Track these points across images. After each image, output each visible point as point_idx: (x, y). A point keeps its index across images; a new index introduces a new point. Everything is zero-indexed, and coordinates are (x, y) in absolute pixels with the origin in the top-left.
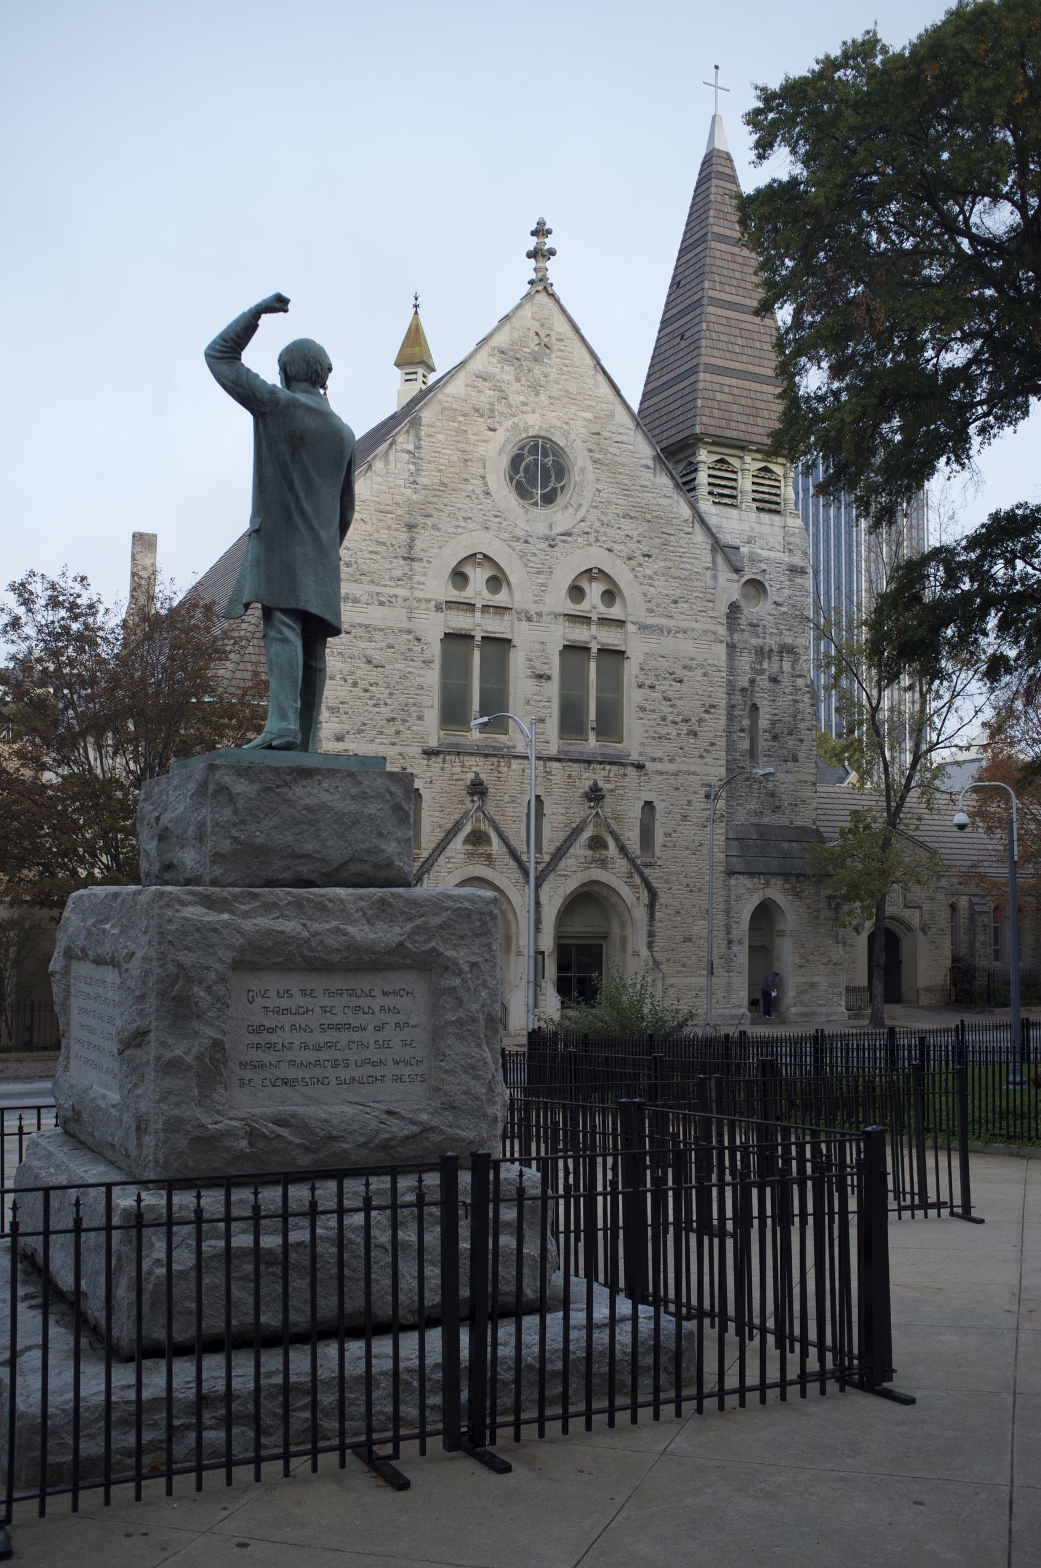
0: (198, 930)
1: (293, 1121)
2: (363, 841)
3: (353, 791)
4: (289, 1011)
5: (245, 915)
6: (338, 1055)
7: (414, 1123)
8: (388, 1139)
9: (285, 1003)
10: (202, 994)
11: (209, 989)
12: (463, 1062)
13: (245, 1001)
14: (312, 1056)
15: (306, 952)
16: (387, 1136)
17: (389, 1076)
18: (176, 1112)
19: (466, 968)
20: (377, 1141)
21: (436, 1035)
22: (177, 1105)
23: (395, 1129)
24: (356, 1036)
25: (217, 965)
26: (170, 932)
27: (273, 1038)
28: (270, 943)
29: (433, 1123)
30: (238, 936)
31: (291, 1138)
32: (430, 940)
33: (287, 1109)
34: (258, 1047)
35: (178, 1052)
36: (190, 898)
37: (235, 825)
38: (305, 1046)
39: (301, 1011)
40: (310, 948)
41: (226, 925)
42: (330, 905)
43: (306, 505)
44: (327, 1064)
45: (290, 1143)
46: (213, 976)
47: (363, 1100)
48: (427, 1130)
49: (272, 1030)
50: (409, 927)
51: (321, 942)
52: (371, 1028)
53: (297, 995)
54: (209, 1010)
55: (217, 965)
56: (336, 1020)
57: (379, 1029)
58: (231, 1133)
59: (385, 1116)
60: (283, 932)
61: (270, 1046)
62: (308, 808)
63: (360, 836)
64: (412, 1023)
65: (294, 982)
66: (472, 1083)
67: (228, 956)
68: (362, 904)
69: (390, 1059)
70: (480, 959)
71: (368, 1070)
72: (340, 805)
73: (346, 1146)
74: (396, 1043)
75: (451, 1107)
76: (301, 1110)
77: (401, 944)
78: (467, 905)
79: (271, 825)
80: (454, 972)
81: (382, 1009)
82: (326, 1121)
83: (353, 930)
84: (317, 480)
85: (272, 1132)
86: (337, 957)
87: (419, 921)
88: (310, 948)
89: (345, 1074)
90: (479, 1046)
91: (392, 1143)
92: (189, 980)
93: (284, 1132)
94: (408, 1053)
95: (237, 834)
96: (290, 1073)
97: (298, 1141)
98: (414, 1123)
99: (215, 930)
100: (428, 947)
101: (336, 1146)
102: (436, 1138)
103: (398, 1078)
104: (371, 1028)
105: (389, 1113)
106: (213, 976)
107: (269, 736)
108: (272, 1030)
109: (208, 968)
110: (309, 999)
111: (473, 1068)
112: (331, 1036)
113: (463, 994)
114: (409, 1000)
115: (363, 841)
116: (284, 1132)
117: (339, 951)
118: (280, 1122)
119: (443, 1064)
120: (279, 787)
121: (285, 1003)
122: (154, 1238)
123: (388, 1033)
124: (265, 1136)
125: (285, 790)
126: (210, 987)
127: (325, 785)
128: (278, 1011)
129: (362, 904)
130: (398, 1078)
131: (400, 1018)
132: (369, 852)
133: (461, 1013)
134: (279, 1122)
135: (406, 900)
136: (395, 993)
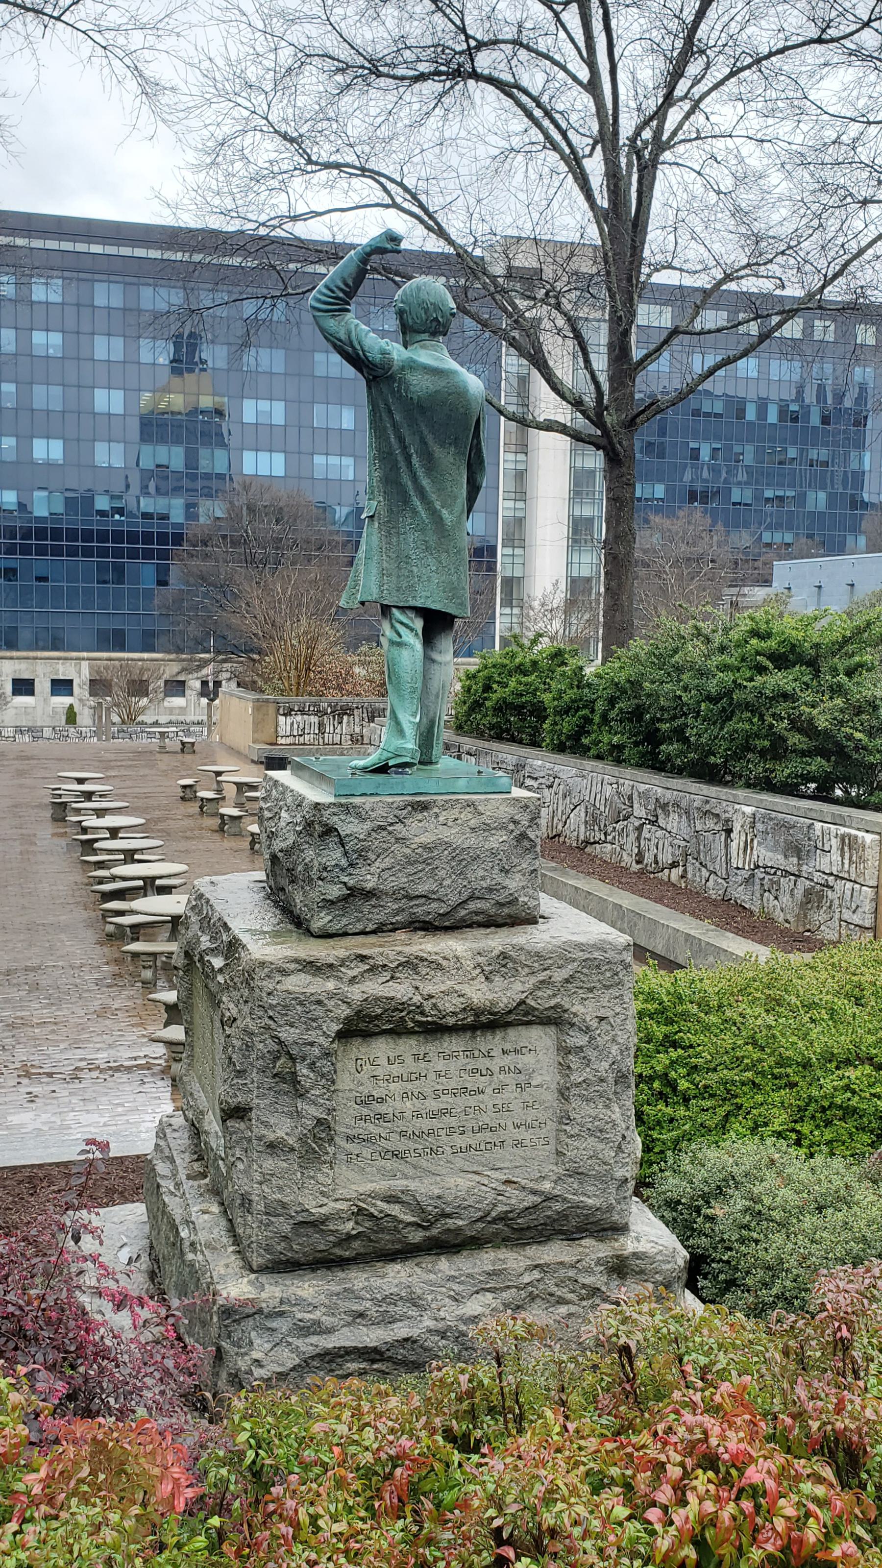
0: (301, 1003)
1: (405, 1198)
2: (483, 878)
3: (473, 823)
4: (400, 1078)
5: (353, 980)
6: (453, 1122)
7: (534, 1192)
8: (507, 1212)
9: (396, 1070)
10: (305, 1071)
11: (312, 1066)
12: (589, 1126)
13: (353, 1070)
14: (425, 1124)
15: (419, 1018)
16: (507, 1208)
17: (509, 1142)
18: (279, 1196)
19: (594, 1024)
20: (494, 1214)
21: (563, 1093)
22: (280, 1189)
23: (513, 1201)
24: (472, 1101)
25: (322, 1039)
26: (272, 1007)
27: (382, 1108)
28: (379, 1011)
29: (556, 1192)
30: (344, 1007)
31: (402, 1217)
32: (554, 995)
33: (399, 1184)
34: (365, 1119)
35: (280, 1133)
36: (293, 966)
37: (343, 870)
38: (417, 1114)
39: (413, 1077)
40: (423, 1013)
41: (332, 996)
42: (445, 963)
43: (425, 482)
44: (441, 1132)
45: (401, 1222)
46: (316, 1051)
47: (480, 1169)
48: (549, 1198)
49: (382, 1100)
50: (533, 980)
51: (434, 1005)
52: (489, 1091)
53: (409, 1060)
54: (312, 1088)
55: (322, 1039)
56: (453, 1084)
57: (498, 1090)
58: (337, 1216)
59: (502, 1187)
60: (392, 998)
61: (381, 1117)
62: (425, 847)
63: (481, 873)
64: (534, 1083)
65: (408, 1046)
66: (601, 1146)
67: (335, 1027)
68: (480, 959)
69: (509, 1124)
70: (610, 1013)
71: (488, 1136)
72: (458, 841)
73: (461, 1223)
74: (516, 1106)
75: (577, 1173)
76: (412, 1185)
77: (523, 1002)
78: (596, 955)
79: (383, 866)
80: (581, 1029)
81: (502, 1069)
82: (439, 1197)
83: (466, 989)
84: (438, 451)
85: (381, 1212)
86: (451, 1021)
87: (542, 976)
88: (423, 1013)
89: (460, 1141)
90: (607, 1107)
91: (511, 1215)
92: (292, 1058)
93: (395, 1210)
94: (530, 1116)
95: (346, 879)
96: (401, 1145)
97: (409, 1218)
98: (534, 1192)
99: (319, 1002)
100: (552, 1003)
101: (451, 1223)
102: (558, 1206)
103: (519, 1144)
104: (489, 1091)
105: (508, 1182)
106: (316, 1051)
107: (386, 755)
108: (382, 1100)
109: (312, 1044)
110: (422, 1064)
111: (601, 1131)
112: (447, 1100)
113: (592, 1054)
114: (540, 1039)
115: (483, 878)
116: (395, 1210)
117: (454, 1014)
118: (391, 1199)
119: (568, 1128)
120: (391, 824)
121: (396, 1070)
122: (253, 1334)
123: (511, 1093)
124: (372, 1215)
125: (398, 827)
126: (314, 1063)
127: (441, 819)
128: (390, 1079)
129: (480, 959)
130: (519, 1144)
131: (522, 1078)
132: (490, 890)
133: (587, 1074)
134: (391, 1199)
135: (529, 953)
136: (516, 1051)
